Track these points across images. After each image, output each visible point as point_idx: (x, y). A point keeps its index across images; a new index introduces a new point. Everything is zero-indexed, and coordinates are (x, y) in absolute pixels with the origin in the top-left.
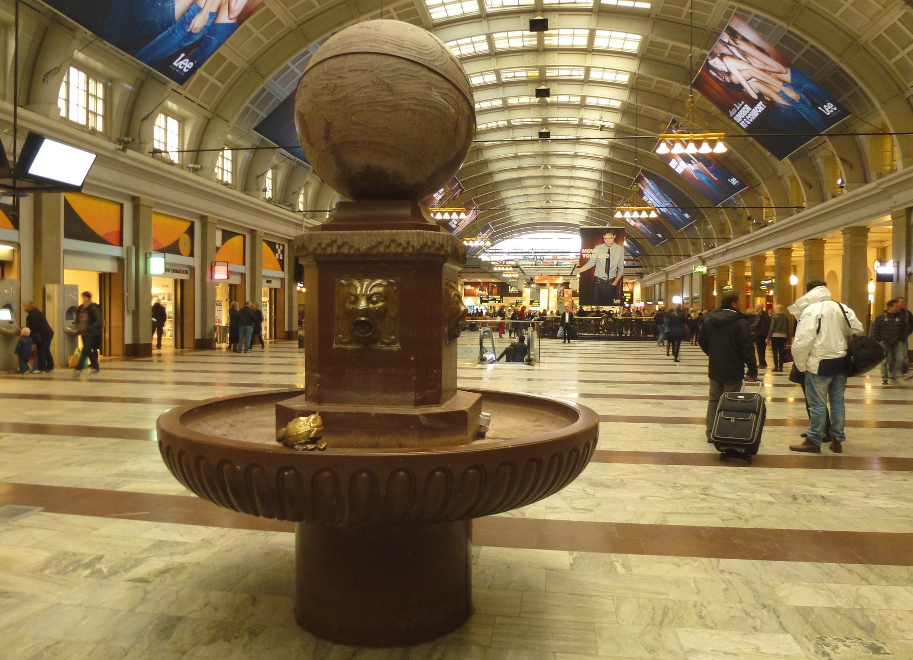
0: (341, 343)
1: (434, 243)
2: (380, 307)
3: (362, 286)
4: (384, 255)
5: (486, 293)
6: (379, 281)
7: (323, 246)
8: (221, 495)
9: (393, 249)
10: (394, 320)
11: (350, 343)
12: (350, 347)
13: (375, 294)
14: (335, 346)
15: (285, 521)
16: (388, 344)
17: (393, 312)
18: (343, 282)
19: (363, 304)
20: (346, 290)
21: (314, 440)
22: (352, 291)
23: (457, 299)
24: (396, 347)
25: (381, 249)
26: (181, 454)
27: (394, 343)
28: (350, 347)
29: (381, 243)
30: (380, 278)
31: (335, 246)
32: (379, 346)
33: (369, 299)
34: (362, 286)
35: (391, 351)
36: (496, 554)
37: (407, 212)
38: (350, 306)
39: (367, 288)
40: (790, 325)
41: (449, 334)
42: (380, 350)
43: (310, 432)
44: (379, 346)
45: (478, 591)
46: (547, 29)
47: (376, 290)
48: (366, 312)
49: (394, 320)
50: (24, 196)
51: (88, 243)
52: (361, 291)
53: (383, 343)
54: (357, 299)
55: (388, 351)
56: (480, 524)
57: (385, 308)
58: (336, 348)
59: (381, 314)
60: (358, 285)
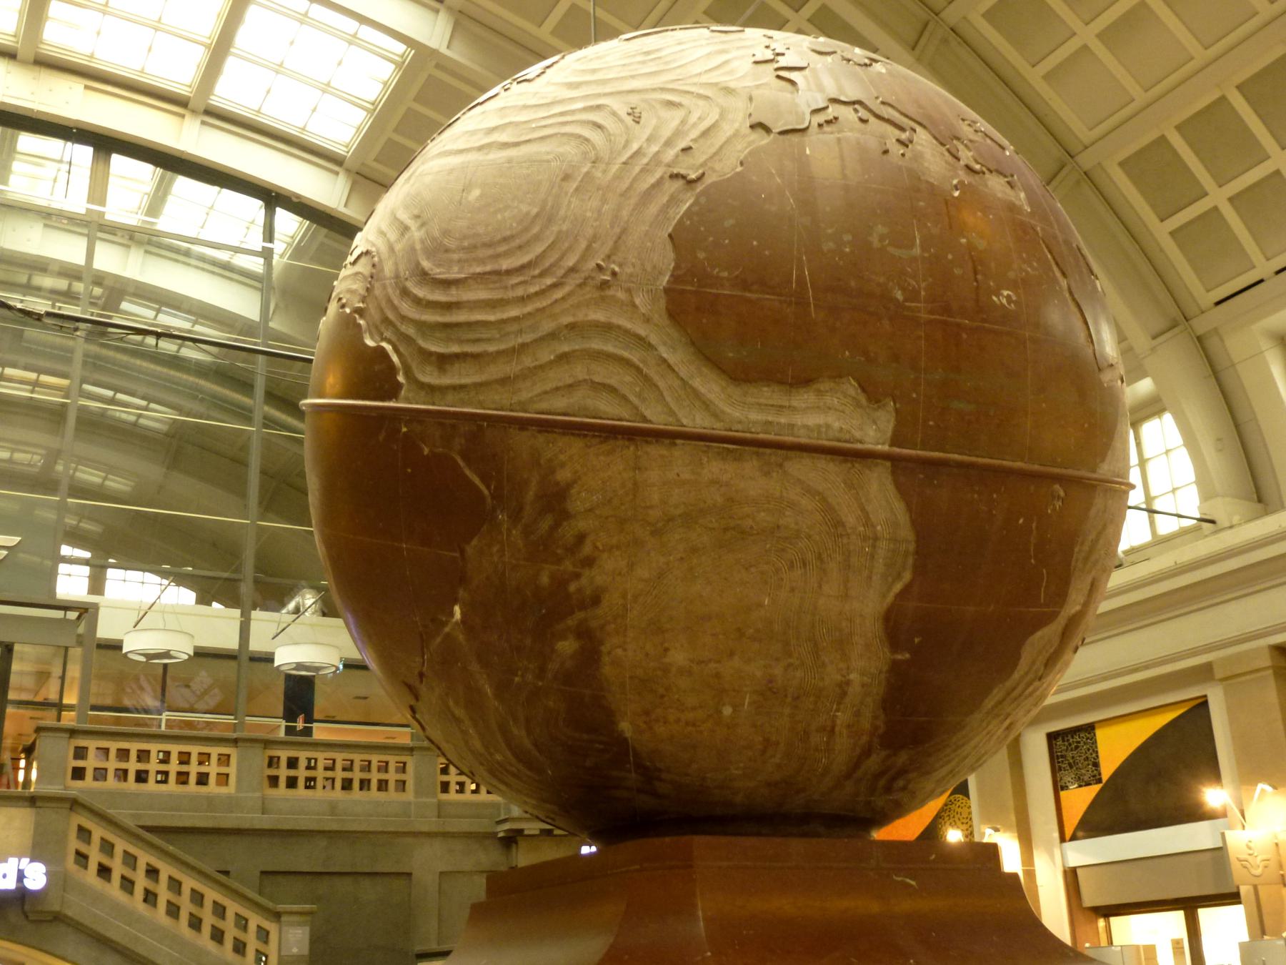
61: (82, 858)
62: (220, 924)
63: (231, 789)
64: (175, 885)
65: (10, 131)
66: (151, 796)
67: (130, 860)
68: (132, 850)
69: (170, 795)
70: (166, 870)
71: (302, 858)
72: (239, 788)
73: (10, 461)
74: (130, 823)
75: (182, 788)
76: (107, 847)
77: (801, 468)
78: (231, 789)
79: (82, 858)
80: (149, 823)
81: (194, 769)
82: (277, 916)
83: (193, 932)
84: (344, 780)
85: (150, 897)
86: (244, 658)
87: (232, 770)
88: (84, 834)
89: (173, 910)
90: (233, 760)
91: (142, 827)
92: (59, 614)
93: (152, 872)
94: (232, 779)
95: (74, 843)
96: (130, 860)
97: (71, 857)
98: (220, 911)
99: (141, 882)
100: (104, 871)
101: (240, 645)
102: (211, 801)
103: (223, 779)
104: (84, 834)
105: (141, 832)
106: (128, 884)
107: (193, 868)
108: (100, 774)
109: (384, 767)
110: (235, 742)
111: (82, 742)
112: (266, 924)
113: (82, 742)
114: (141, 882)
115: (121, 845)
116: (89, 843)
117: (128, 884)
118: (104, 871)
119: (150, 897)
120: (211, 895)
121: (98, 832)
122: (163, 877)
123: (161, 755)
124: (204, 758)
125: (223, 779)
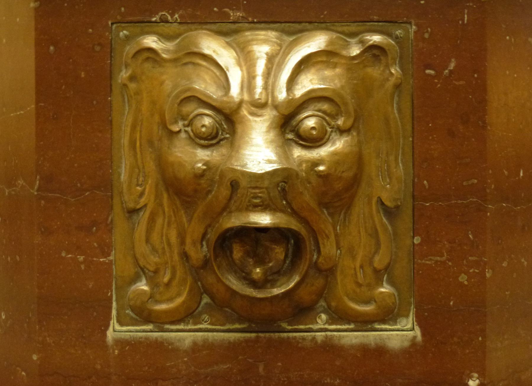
0: (144, 316)
2: (337, 159)
3: (246, 59)
5: (414, 44)
6: (316, 42)
11: (186, 315)
12: (184, 336)
13: (312, 98)
14: (116, 331)
16: (364, 323)
17: (389, 181)
18: (151, 41)
19: (259, 153)
20: (169, 81)
22: (205, 85)
24: (401, 333)
27: (388, 315)
28: (184, 336)
32: (321, 328)
33: (287, 125)
34: (246, 59)
35: (380, 351)
39: (271, 72)
40: (397, 35)
42: (330, 348)
44: (321, 328)
47: (308, 83)
48: (279, 187)
49: (391, 213)
50: (277, 98)
52: (248, 84)
53: (340, 316)
54: (228, 124)
55: (365, 350)
57: (357, 161)
58: (120, 343)
59: (337, 191)
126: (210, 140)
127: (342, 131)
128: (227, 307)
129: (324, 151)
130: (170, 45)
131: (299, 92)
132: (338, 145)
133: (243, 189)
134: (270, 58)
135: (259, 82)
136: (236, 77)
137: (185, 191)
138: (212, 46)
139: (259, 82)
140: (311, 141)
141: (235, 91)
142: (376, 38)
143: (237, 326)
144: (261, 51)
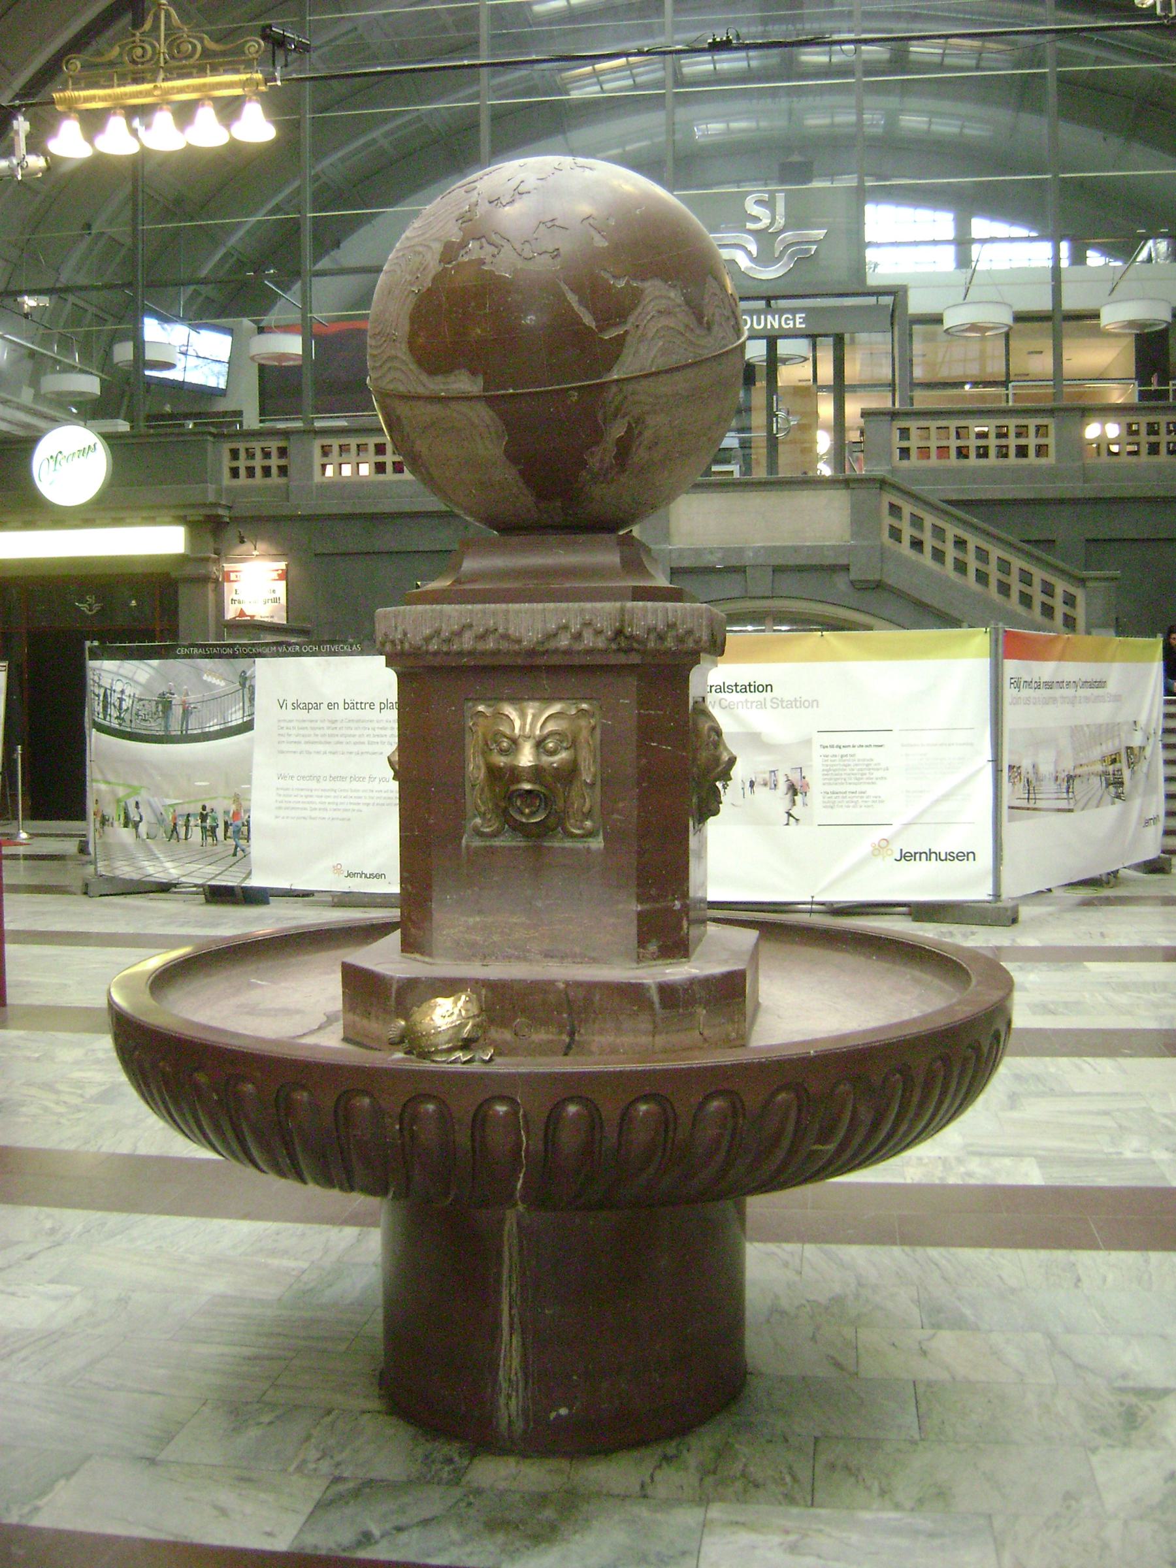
0: (482, 835)
1: (672, 626)
2: (563, 762)
3: (523, 716)
4: (568, 652)
6: (556, 708)
7: (445, 634)
8: (235, 1145)
9: (589, 640)
10: (593, 785)
15: (354, 1195)
18: (481, 708)
19: (526, 758)
21: (467, 1044)
23: (714, 736)
25: (564, 642)
26: (169, 1065)
27: (590, 834)
29: (566, 627)
30: (560, 699)
31: (468, 636)
33: (539, 744)
34: (523, 716)
36: (792, 1262)
37: (608, 557)
38: (501, 761)
41: (699, 807)
43: (461, 1026)
45: (758, 1346)
46: (1137, 335)
47: (551, 727)
48: (537, 772)
51: (1096, 1027)
54: (515, 743)
56: (757, 1205)
59: (569, 774)
60: (513, 714)
61: (896, 534)
62: (1027, 590)
63: (1050, 460)
64: (982, 555)
65: (6, 935)
66: (975, 470)
67: (939, 532)
68: (940, 523)
69: (992, 468)
70: (973, 541)
71: (1126, 526)
72: (1058, 459)
73: (832, 125)
74: (934, 499)
75: (1002, 462)
76: (917, 522)
77: (454, 405)
78: (1050, 460)
79: (896, 534)
80: (955, 497)
81: (1012, 442)
82: (1082, 582)
83: (1004, 598)
84: (384, 454)
85: (961, 567)
86: (1058, 317)
87: (1051, 441)
88: (895, 510)
89: (982, 577)
90: (1052, 430)
91: (943, 501)
92: (871, 300)
93: (960, 543)
94: (1052, 450)
95: (888, 520)
96: (939, 532)
97: (886, 533)
98: (1026, 578)
99: (951, 553)
100: (917, 544)
101: (1054, 304)
102: (1033, 474)
103: (1041, 450)
104: (895, 510)
105: (944, 506)
106: (938, 555)
107: (999, 539)
108: (924, 452)
109: (1021, 432)
110: (1051, 412)
111: (904, 424)
112: (1072, 590)
113: (904, 424)
114: (951, 553)
115: (929, 520)
116: (900, 518)
117: (938, 555)
118: (917, 544)
119: (961, 567)
120: (1017, 563)
121: (907, 509)
122: (971, 547)
123: (1134, 427)
124: (1021, 432)
125: (1041, 450)
126: (503, 752)
127: (567, 749)
128: (518, 828)
129: (556, 758)
130: (491, 709)
131: (546, 731)
132: (564, 755)
133: (515, 774)
134: (534, 716)
135: (528, 727)
136: (517, 724)
137: (494, 773)
138: (510, 711)
139: (528, 727)
140: (552, 753)
141: (517, 731)
142: (584, 706)
143: (937, 1092)
144: (530, 713)
